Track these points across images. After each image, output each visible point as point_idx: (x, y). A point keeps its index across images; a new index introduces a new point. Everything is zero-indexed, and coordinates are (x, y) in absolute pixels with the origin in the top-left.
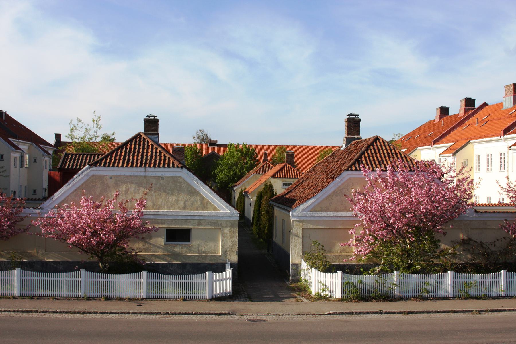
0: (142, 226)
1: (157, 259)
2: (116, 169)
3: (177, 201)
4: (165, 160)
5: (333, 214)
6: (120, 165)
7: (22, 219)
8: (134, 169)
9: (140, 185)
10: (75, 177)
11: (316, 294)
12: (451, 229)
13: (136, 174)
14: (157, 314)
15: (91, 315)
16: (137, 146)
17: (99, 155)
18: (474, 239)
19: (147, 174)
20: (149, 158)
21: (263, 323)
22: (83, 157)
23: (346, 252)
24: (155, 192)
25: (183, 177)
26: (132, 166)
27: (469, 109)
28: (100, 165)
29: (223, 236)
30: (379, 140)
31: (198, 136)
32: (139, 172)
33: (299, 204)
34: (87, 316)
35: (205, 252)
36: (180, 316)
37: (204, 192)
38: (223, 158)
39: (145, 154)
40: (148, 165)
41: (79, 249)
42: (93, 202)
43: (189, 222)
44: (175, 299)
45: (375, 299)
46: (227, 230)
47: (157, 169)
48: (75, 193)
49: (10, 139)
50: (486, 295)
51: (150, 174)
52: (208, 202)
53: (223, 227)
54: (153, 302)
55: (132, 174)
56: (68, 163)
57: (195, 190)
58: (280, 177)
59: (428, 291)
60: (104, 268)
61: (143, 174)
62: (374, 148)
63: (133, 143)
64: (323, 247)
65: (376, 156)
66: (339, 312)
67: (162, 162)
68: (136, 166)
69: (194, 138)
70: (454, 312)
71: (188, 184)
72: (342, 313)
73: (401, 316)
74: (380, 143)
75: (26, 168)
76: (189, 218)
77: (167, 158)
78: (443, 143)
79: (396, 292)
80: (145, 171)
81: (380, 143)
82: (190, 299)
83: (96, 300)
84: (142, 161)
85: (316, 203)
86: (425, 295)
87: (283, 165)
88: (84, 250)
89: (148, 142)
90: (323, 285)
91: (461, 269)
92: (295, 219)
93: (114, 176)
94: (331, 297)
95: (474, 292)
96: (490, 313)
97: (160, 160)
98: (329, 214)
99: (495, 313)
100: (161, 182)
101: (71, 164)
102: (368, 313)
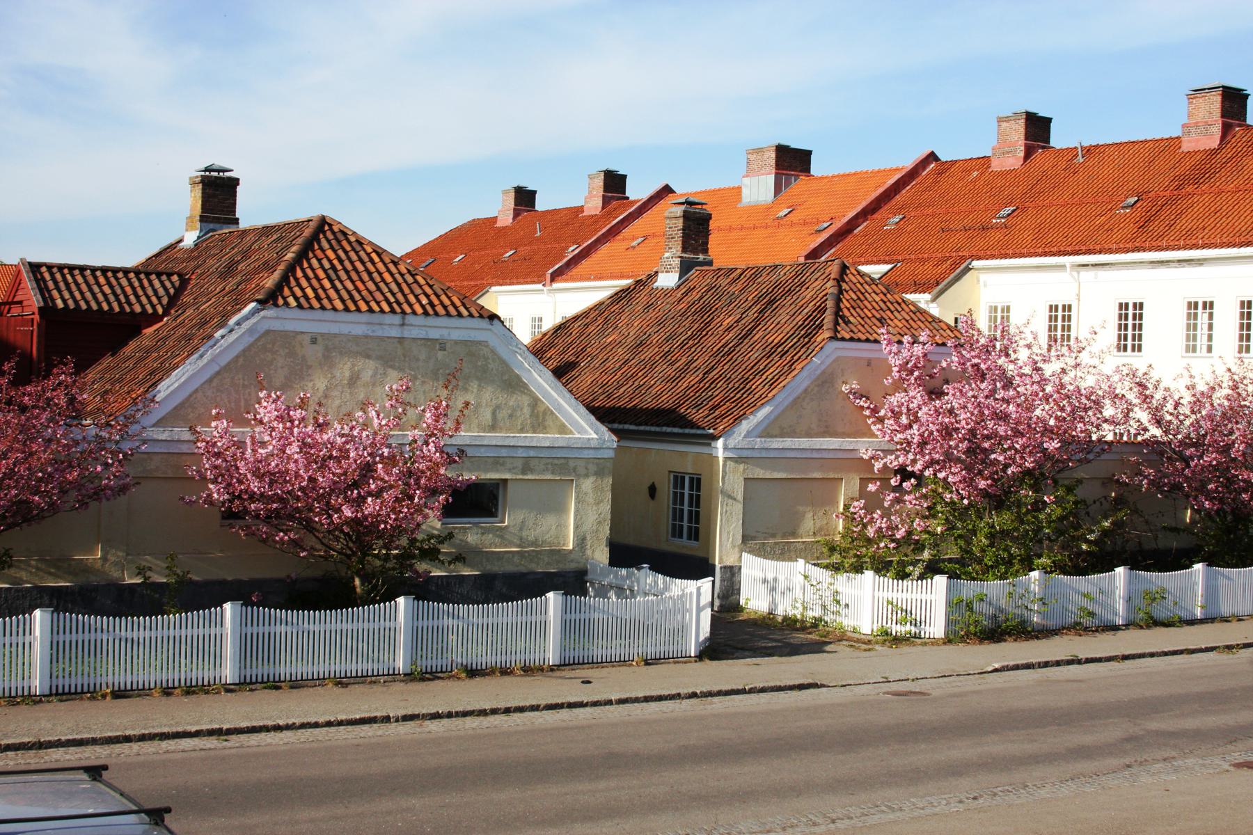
5: (805, 443)
9: (388, 361)
24: (423, 382)
25: (491, 344)
27: (612, 198)
29: (578, 502)
32: (390, 326)
35: (534, 543)
37: (540, 387)
46: (588, 484)
52: (547, 412)
53: (579, 476)
57: (518, 378)
61: (395, 332)
76: (504, 453)
78: (566, 281)
80: (403, 325)
83: (439, 678)
85: (776, 413)
92: (731, 455)
93: (322, 335)
95: (1159, 612)
100: (440, 354)
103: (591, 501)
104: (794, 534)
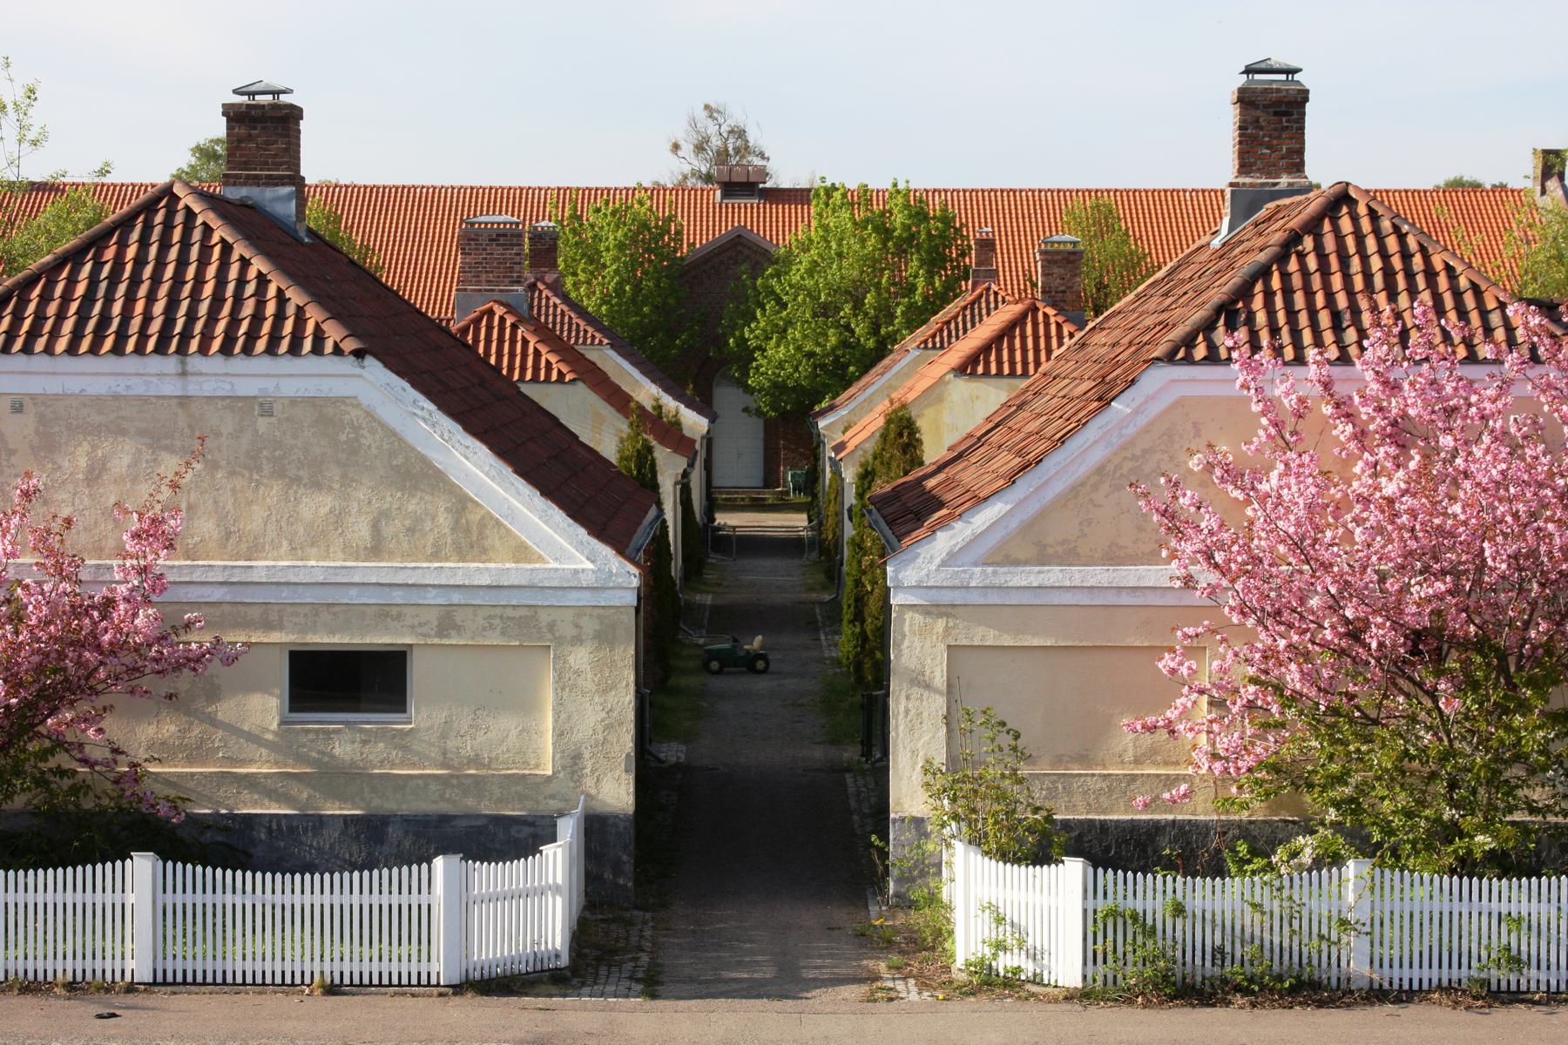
0: (162, 639)
1: (246, 795)
2: (39, 362)
3: (338, 518)
4: (280, 317)
5: (1099, 575)
6: (61, 345)
8: (130, 363)
9: (157, 439)
11: (968, 964)
13: (139, 387)
16: (153, 250)
19: (194, 388)
20: (203, 308)
23: (1166, 763)
24: (233, 474)
25: (364, 401)
30: (1352, 203)
31: (695, 138)
32: (149, 377)
35: (475, 761)
40: (194, 345)
43: (399, 617)
44: (288, 986)
45: (1246, 992)
46: (580, 657)
47: (239, 364)
51: (208, 387)
52: (489, 523)
53: (560, 641)
55: (122, 391)
57: (425, 461)
58: (1000, 374)
61: (171, 388)
63: (135, 235)
64: (1017, 737)
65: (1327, 286)
67: (267, 327)
68: (140, 350)
69: (676, 147)
71: (392, 433)
74: (1355, 219)
76: (398, 597)
77: (291, 310)
79: (1357, 963)
80: (184, 374)
81: (1355, 219)
82: (361, 987)
84: (169, 321)
85: (1014, 523)
86: (1501, 976)
87: (1019, 308)
89: (208, 230)
90: (1000, 920)
93: (33, 397)
94: (1036, 980)
97: (257, 318)
100: (263, 424)
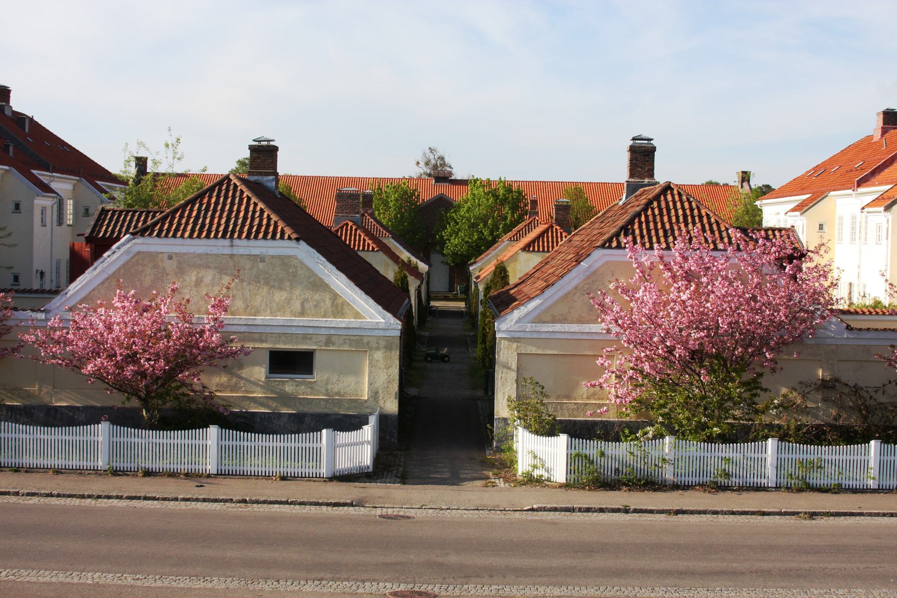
0: (222, 345)
2: (179, 241)
3: (289, 301)
4: (268, 225)
5: (575, 328)
6: (187, 234)
7: (8, 330)
8: (212, 242)
9: (222, 270)
10: (105, 255)
11: (523, 473)
12: (794, 360)
13: (215, 251)
14: (225, 501)
15: (111, 500)
16: (222, 199)
17: (155, 212)
18: (844, 380)
19: (235, 251)
20: (240, 221)
21: (403, 521)
22: (133, 216)
23: (599, 399)
24: (249, 284)
25: (299, 257)
26: (208, 237)
28: (150, 235)
30: (672, 189)
31: (425, 160)
32: (219, 247)
33: (516, 307)
34: (103, 503)
35: (338, 394)
36: (265, 506)
37: (337, 285)
38: (459, 206)
39: (234, 214)
40: (236, 235)
41: (106, 386)
42: (136, 302)
43: (311, 339)
44: (267, 477)
45: (627, 485)
46: (379, 355)
47: (252, 243)
48: (106, 284)
49: (34, 172)
50: (839, 485)
51: (241, 251)
52: (345, 303)
53: (371, 349)
54: (228, 481)
56: (104, 228)
57: (321, 280)
59: (728, 475)
60: (150, 419)
61: (227, 251)
62: (659, 206)
63: (215, 194)
64: (543, 388)
66: (549, 506)
69: (418, 163)
70: (764, 514)
71: (309, 269)
72: (555, 509)
73: (662, 517)
74: (673, 195)
75: (69, 225)
76: (310, 331)
77: (272, 222)
78: (874, 185)
79: (668, 474)
80: (232, 246)
81: (673, 195)
82: (294, 478)
83: (128, 475)
84: (227, 226)
85: (543, 308)
86: (722, 480)
87: (546, 226)
88: (121, 385)
89: (242, 192)
90: (535, 457)
91: (815, 436)
93: (176, 254)
94: (549, 480)
95: (817, 479)
96: (831, 518)
98: (567, 327)
99: (842, 518)
100: (261, 265)
101: (110, 229)
102: (601, 510)
103: (382, 366)
104: (568, 397)
